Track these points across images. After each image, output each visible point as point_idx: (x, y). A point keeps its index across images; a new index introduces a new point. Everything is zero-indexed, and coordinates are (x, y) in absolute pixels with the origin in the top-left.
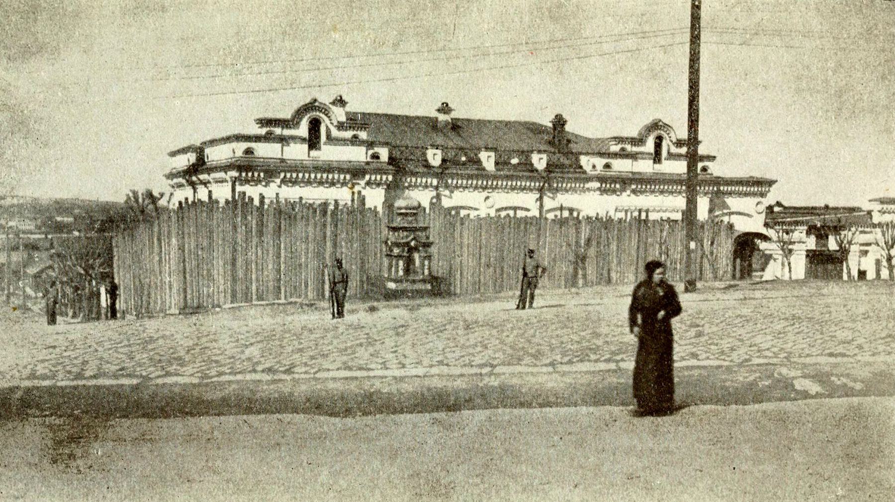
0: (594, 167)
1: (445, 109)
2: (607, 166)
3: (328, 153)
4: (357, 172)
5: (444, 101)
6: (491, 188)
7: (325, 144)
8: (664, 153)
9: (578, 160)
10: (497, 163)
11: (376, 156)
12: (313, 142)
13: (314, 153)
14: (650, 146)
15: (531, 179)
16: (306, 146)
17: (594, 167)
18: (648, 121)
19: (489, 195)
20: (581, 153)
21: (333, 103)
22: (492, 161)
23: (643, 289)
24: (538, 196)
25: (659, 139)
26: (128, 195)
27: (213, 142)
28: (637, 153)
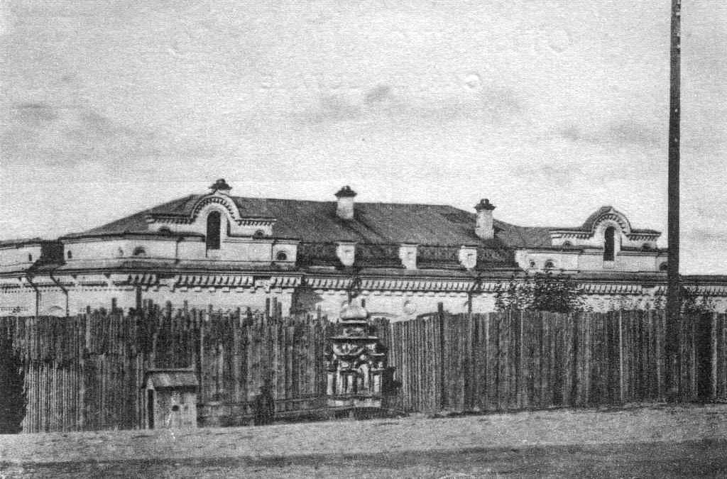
0: (533, 264)
1: (486, 206)
2: (549, 264)
3: (228, 252)
4: (260, 273)
5: (484, 198)
6: (186, 285)
7: (619, 255)
8: (223, 235)
9: (513, 256)
10: (419, 260)
11: (282, 256)
12: (608, 253)
13: (212, 253)
14: (598, 239)
15: (459, 279)
16: (203, 245)
17: (533, 264)
18: (594, 209)
19: (410, 298)
20: (517, 248)
21: (478, 208)
22: (414, 256)
23: (550, 407)
24: (467, 299)
25: (609, 232)
26: (238, 311)
27: (74, 238)
28: (586, 247)
